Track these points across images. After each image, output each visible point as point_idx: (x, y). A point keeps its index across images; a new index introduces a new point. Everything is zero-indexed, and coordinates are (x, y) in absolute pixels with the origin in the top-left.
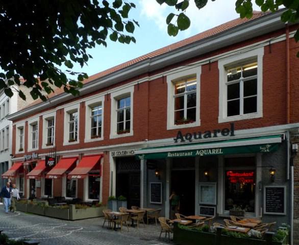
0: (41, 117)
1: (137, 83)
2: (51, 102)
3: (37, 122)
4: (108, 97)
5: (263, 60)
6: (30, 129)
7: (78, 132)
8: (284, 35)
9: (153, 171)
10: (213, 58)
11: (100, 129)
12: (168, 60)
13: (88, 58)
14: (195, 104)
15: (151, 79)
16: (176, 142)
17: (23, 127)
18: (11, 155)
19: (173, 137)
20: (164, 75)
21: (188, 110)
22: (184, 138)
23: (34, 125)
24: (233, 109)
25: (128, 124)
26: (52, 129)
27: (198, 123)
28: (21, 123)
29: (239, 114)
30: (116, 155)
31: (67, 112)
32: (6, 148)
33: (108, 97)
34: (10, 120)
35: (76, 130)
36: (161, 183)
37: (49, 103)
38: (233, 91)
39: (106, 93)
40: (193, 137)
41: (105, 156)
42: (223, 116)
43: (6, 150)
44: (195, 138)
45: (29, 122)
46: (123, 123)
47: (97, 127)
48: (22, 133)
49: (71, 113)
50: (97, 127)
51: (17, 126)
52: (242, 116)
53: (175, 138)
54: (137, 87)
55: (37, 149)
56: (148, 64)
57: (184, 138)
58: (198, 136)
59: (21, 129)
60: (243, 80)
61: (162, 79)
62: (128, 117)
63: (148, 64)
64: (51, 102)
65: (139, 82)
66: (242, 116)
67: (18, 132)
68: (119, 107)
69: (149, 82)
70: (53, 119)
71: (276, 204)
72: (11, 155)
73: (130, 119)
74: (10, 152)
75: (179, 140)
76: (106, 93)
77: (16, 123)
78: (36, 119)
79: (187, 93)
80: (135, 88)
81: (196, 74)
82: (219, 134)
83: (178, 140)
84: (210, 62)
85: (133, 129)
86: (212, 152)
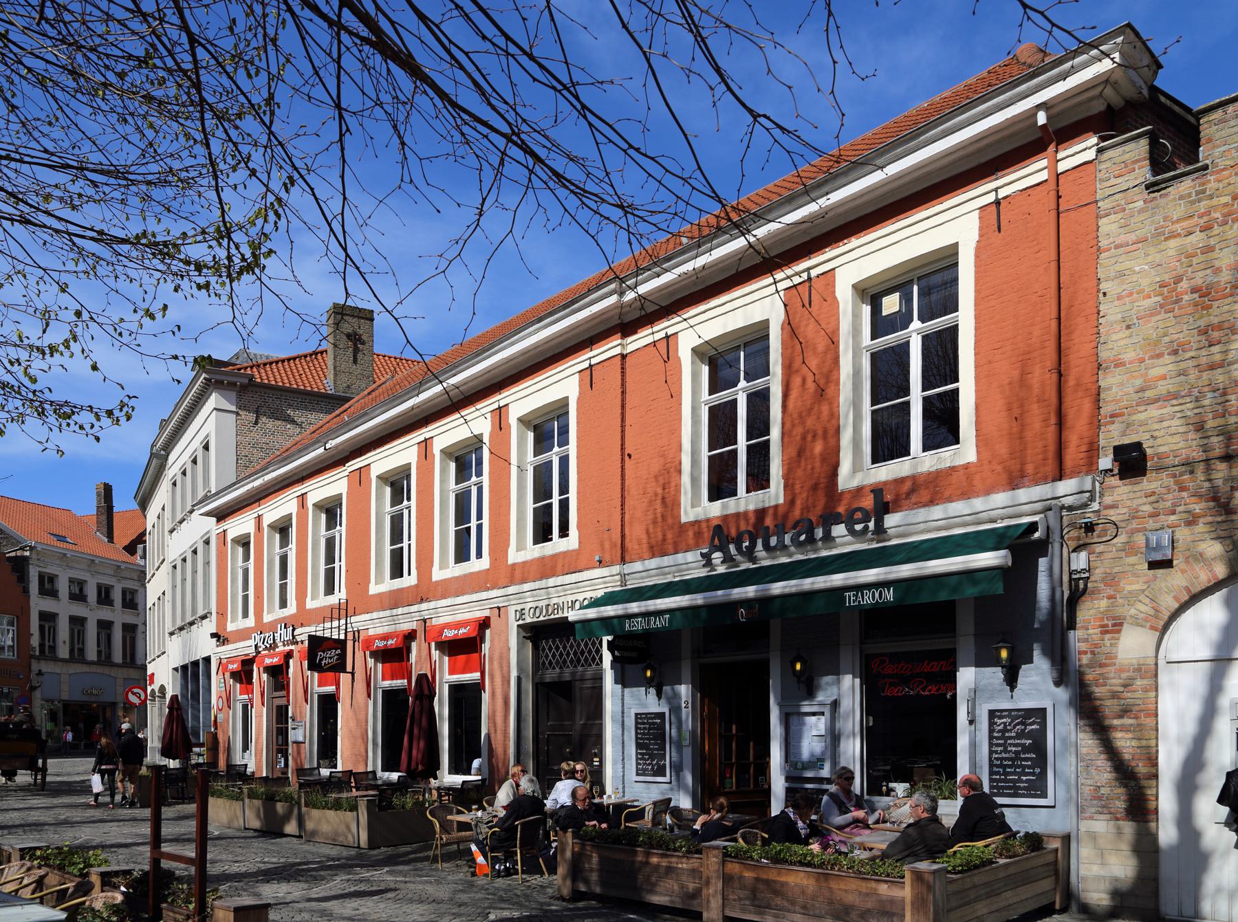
1: (991, 198)
2: (328, 446)
3: (407, 467)
5: (977, 256)
6: (317, 527)
7: (573, 495)
8: (1044, 163)
9: (641, 666)
10: (816, 264)
11: (564, 505)
12: (297, 468)
14: (953, 375)
15: (630, 349)
17: (248, 535)
18: (213, 635)
19: (697, 546)
20: (670, 331)
21: (925, 399)
22: (732, 548)
24: (890, 442)
25: (759, 455)
26: (406, 512)
27: (775, 493)
28: (242, 525)
29: (906, 452)
30: (529, 620)
31: (520, 420)
32: (201, 612)
34: (208, 514)
36: (666, 710)
37: (321, 450)
38: (888, 373)
40: (760, 542)
42: (856, 471)
44: (767, 547)
45: (312, 499)
46: (735, 452)
48: (285, 542)
50: (473, 524)
52: (921, 460)
53: (704, 551)
56: (613, 299)
57: (732, 548)
58: (773, 541)
61: (994, 207)
62: (758, 425)
63: (613, 299)
64: (328, 446)
65: (594, 361)
66: (921, 460)
70: (408, 477)
71: (1024, 767)
72: (213, 635)
73: (767, 432)
76: (496, 406)
79: (744, 390)
80: (581, 381)
81: (567, 398)
83: (714, 556)
84: (810, 279)
85: (579, 527)
86: (1147, 540)
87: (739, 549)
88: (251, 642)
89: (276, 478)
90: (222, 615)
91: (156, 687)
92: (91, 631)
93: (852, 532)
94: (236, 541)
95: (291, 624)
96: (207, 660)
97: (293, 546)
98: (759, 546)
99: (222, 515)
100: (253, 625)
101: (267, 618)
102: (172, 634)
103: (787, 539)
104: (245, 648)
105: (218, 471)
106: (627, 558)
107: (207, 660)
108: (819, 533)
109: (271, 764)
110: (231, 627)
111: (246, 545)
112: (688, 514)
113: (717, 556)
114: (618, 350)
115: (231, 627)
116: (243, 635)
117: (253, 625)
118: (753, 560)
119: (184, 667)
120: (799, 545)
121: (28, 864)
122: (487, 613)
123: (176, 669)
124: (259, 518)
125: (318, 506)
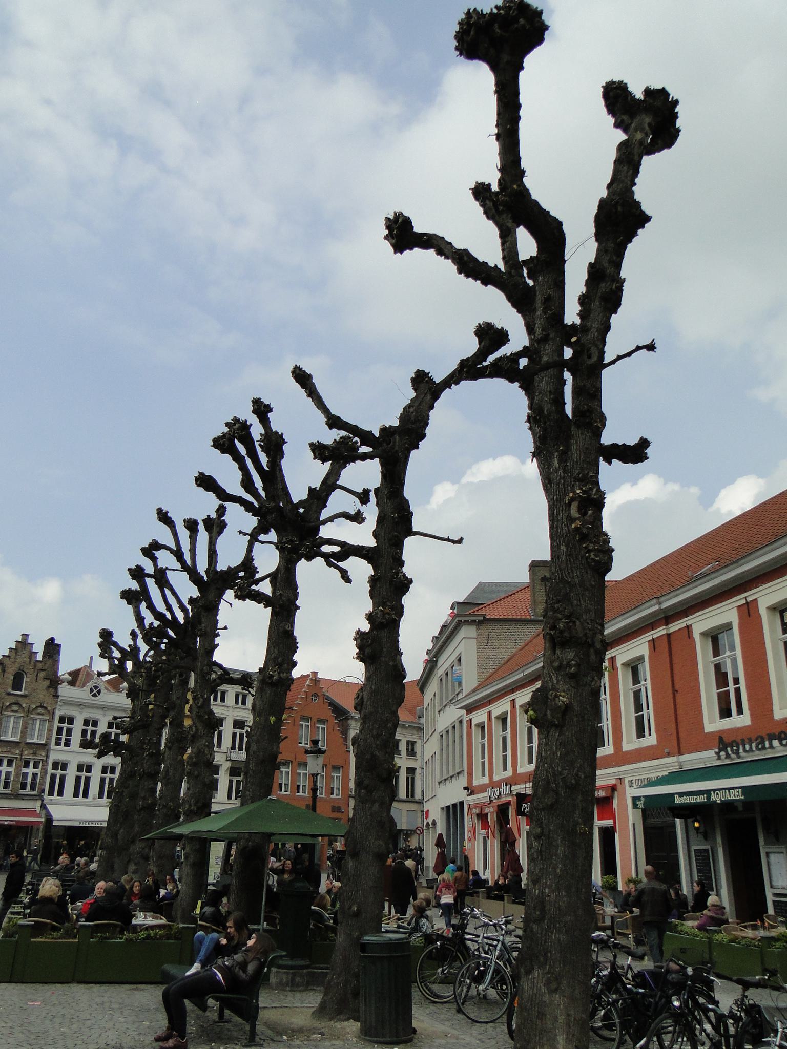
0: (513, 701)
1: (744, 602)
3: (506, 713)
4: (749, 611)
6: (496, 727)
10: (750, 595)
11: (738, 691)
13: (358, 707)
15: (672, 630)
16: (719, 758)
18: (465, 788)
22: (729, 749)
23: (503, 719)
28: (480, 717)
29: (731, 716)
31: (623, 664)
32: (458, 770)
33: (749, 611)
34: (461, 708)
35: (736, 681)
39: (740, 599)
41: (619, 787)
43: (458, 773)
44: (745, 751)
47: (731, 688)
48: (504, 729)
49: (714, 637)
51: (474, 723)
54: (653, 643)
55: (509, 773)
57: (729, 749)
59: (481, 726)
60: (728, 657)
65: (654, 636)
67: (476, 734)
68: (716, 653)
69: (669, 635)
72: (465, 788)
74: (463, 781)
75: (723, 754)
76: (650, 638)
77: (471, 716)
78: (501, 707)
80: (649, 646)
82: (776, 743)
87: (732, 750)
88: (486, 794)
89: (625, 626)
90: (470, 775)
91: (430, 821)
92: (107, 782)
93: (782, 744)
94: (477, 725)
95: (509, 782)
96: (462, 803)
97: (509, 730)
98: (741, 750)
99: (470, 709)
100: (488, 782)
101: (496, 778)
102: (439, 783)
103: (754, 745)
104: (483, 797)
105: (470, 677)
106: (682, 750)
107: (462, 803)
108: (767, 744)
109: (504, 875)
110: (475, 783)
111: (483, 728)
112: (709, 727)
113: (723, 754)
114: (664, 632)
115: (475, 783)
116: (482, 788)
117: (488, 782)
118: (739, 757)
119: (448, 807)
120: (758, 749)
121: (284, 599)
122: (614, 782)
123: (443, 808)
124: (490, 712)
125: (497, 718)
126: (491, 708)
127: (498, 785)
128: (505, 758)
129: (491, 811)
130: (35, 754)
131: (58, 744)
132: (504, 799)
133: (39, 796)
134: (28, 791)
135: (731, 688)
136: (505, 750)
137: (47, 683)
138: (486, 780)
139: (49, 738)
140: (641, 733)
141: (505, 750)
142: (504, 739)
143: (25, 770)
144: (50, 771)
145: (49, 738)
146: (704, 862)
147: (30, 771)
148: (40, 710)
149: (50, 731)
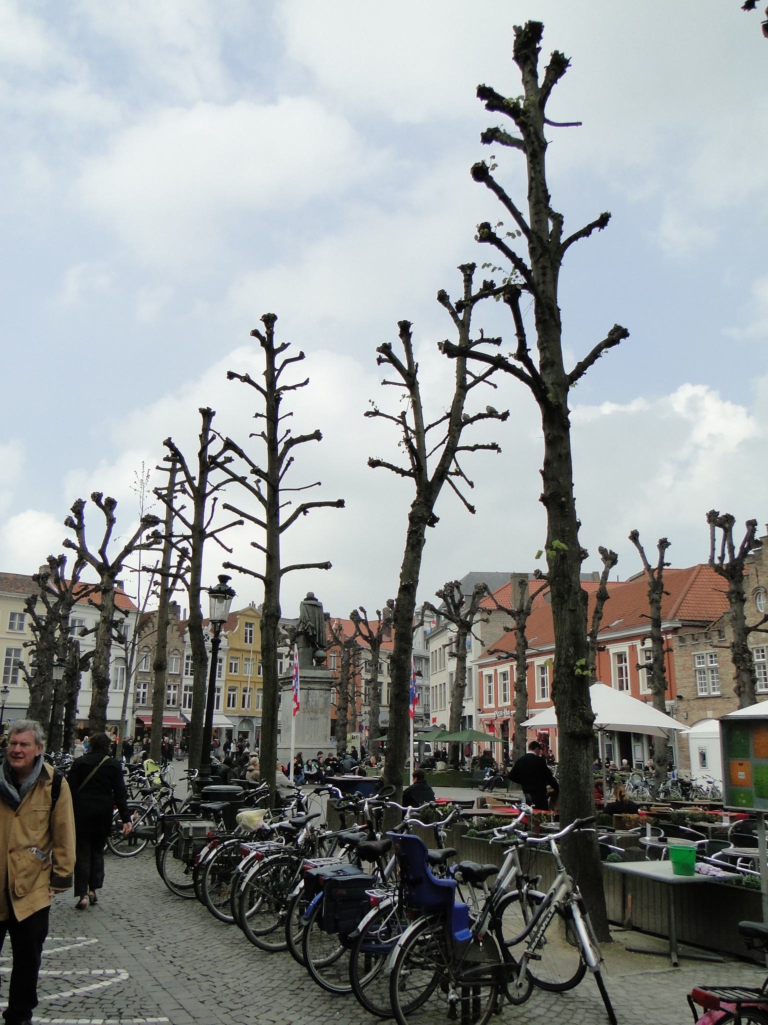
6: (500, 679)
59: (490, 677)
67: (485, 681)
126: (496, 667)
127: (502, 709)
128: (490, 697)
129: (497, 725)
130: (174, 681)
131: (186, 674)
132: (505, 717)
133: (178, 709)
134: (171, 705)
135: (624, 678)
136: (490, 692)
137: (179, 633)
138: (493, 706)
139: (181, 670)
140: (505, 700)
141: (490, 692)
142: (490, 687)
143: (138, 690)
144: (184, 692)
145: (181, 670)
146: (610, 749)
147: (141, 690)
148: (176, 652)
149: (182, 665)
